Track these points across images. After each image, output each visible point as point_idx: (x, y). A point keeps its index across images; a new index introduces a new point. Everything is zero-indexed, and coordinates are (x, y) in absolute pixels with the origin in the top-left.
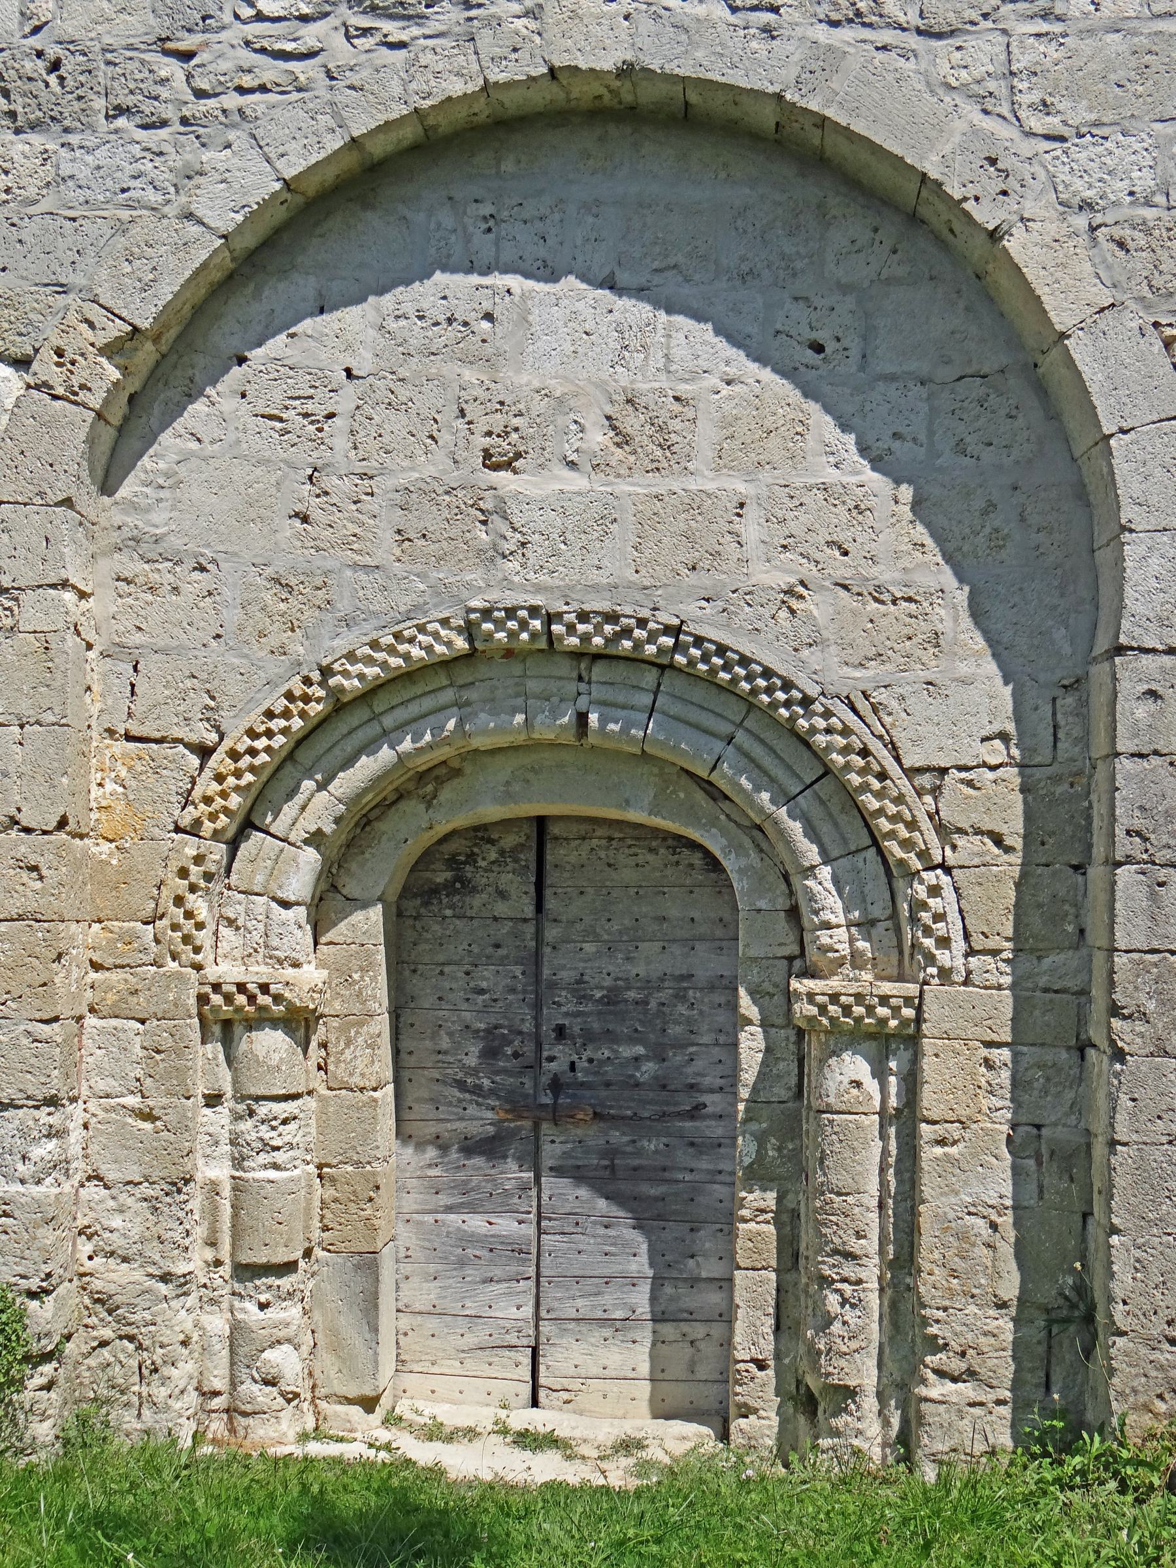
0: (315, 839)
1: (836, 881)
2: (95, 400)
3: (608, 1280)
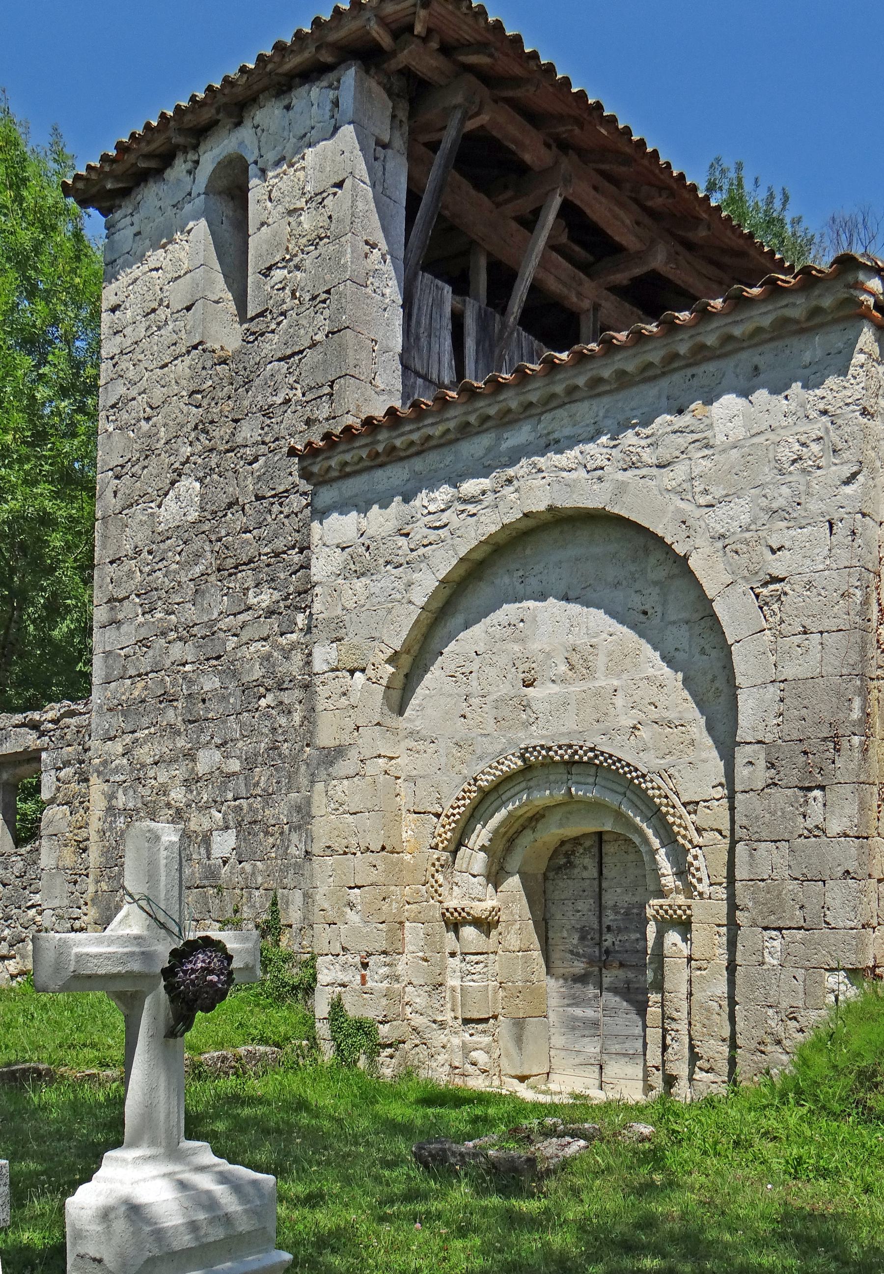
0: (483, 848)
1: (667, 855)
2: (384, 682)
3: (627, 1037)
